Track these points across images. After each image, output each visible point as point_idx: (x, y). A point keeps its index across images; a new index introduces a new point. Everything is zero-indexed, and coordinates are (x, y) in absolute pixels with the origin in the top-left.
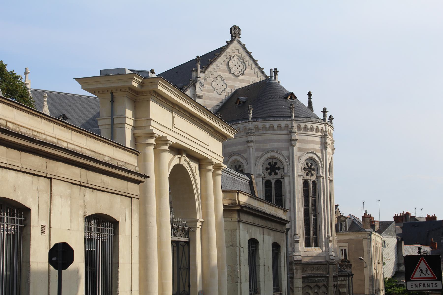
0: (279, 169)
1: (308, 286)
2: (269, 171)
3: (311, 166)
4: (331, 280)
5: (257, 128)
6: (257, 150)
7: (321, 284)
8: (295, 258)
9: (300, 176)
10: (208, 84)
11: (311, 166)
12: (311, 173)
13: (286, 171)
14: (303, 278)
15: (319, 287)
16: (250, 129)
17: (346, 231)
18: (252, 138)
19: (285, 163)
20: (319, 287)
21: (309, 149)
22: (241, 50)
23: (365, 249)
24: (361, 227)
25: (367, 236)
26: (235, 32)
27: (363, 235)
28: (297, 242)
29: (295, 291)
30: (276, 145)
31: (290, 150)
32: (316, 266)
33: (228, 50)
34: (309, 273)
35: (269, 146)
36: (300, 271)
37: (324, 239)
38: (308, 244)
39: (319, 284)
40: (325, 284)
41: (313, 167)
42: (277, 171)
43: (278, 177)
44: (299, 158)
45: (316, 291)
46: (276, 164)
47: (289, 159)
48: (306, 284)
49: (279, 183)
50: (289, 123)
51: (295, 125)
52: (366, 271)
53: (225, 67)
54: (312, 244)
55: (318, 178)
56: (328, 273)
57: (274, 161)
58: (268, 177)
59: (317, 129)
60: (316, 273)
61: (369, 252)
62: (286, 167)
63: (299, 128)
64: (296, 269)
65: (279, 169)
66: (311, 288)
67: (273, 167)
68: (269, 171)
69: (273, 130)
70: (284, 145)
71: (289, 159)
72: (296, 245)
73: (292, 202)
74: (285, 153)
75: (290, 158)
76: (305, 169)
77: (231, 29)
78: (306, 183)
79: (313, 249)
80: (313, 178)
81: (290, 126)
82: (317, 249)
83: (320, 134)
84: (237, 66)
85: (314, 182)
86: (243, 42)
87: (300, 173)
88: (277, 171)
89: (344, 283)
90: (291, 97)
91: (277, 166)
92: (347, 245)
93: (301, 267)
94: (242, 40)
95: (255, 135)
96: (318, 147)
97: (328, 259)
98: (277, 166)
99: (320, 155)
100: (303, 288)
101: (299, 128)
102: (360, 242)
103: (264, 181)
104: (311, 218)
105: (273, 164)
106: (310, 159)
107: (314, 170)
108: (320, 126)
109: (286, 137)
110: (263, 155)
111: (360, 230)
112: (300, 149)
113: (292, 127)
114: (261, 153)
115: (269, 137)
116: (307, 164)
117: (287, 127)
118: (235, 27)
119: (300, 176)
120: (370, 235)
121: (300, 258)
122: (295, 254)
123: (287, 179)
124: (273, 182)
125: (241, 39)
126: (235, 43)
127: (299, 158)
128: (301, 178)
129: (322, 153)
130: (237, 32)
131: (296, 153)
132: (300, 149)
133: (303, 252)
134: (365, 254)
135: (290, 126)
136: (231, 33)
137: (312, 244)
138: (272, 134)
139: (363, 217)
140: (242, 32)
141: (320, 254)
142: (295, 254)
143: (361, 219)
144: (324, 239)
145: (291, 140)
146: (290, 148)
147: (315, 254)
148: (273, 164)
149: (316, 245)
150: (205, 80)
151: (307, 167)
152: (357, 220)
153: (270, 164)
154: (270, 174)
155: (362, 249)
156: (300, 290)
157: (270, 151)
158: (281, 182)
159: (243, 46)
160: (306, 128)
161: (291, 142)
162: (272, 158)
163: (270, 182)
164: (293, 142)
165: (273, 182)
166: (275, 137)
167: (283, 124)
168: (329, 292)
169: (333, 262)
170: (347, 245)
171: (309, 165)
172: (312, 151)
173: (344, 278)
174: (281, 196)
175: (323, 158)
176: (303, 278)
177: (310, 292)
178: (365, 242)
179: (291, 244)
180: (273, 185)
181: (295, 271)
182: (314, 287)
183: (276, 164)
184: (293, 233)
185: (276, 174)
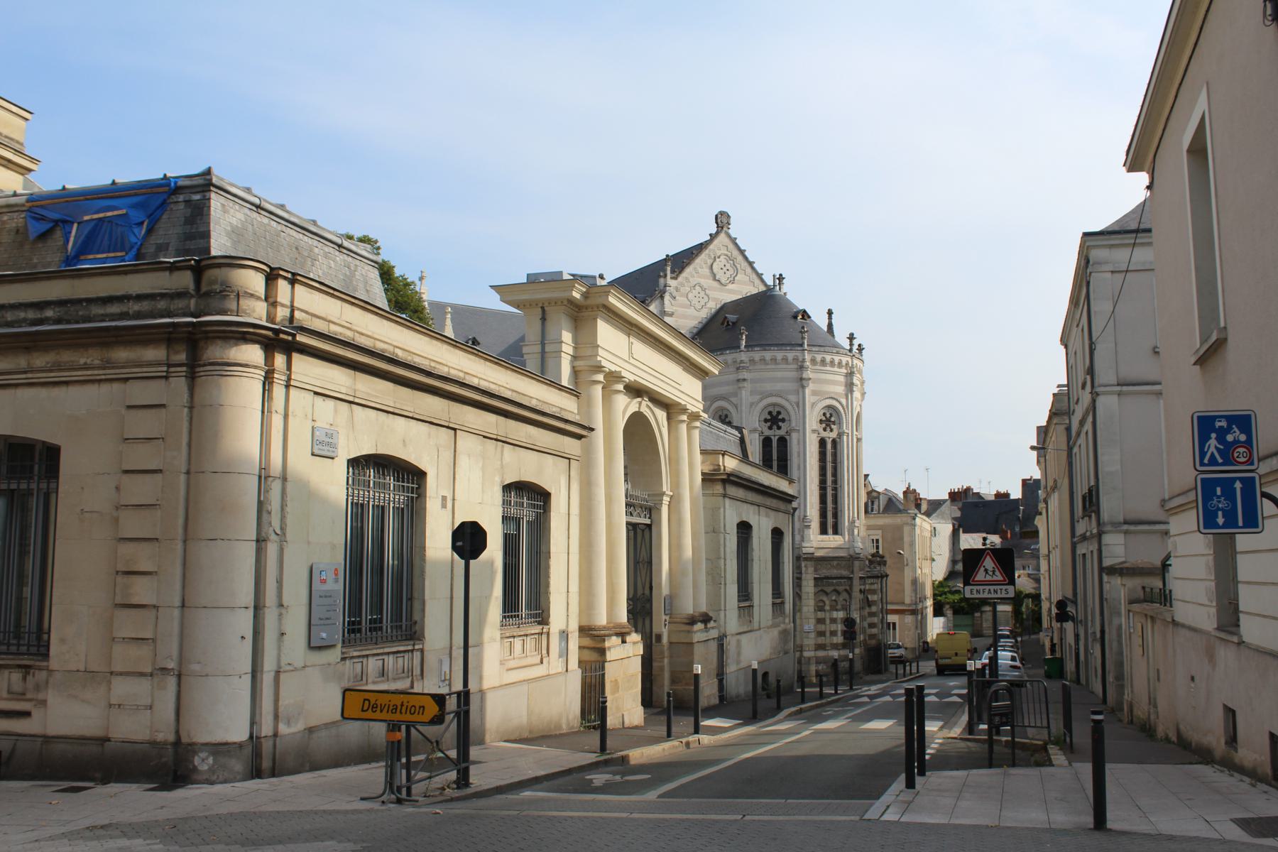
3: (830, 418)
4: (856, 582)
5: (752, 361)
8: (805, 550)
9: (814, 431)
11: (830, 418)
13: (793, 424)
15: (838, 593)
16: (742, 362)
19: (792, 413)
22: (731, 246)
23: (906, 539)
25: (909, 520)
26: (722, 221)
28: (808, 527)
30: (779, 386)
33: (711, 247)
34: (824, 572)
35: (768, 387)
36: (811, 570)
38: (824, 531)
43: (782, 433)
44: (813, 405)
46: (779, 413)
49: (783, 441)
50: (799, 354)
51: (807, 357)
52: (907, 572)
53: (706, 271)
54: (830, 531)
55: (840, 435)
58: (767, 433)
59: (840, 364)
60: (835, 572)
61: (912, 544)
62: (793, 418)
63: (813, 361)
65: (783, 420)
66: (827, 594)
67: (774, 419)
70: (792, 386)
72: (806, 531)
74: (793, 398)
75: (800, 405)
76: (821, 421)
78: (822, 443)
80: (834, 435)
82: (837, 537)
85: (834, 441)
86: (733, 236)
87: (815, 427)
89: (875, 587)
94: (733, 232)
95: (750, 371)
96: (841, 389)
99: (844, 401)
101: (813, 361)
102: (899, 529)
104: (830, 492)
106: (829, 407)
108: (845, 359)
109: (794, 374)
110: (761, 400)
111: (900, 511)
112: (814, 393)
113: (804, 360)
117: (796, 359)
118: (722, 213)
119: (814, 431)
121: (811, 550)
123: (794, 435)
124: (775, 440)
126: (722, 235)
127: (813, 405)
132: (814, 393)
133: (816, 542)
134: (906, 546)
137: (830, 531)
138: (773, 370)
140: (732, 221)
141: (383, 350)
143: (901, 496)
145: (801, 379)
149: (836, 532)
150: (677, 289)
152: (895, 496)
153: (770, 413)
154: (770, 428)
155: (902, 538)
156: (811, 596)
157: (771, 395)
159: (734, 241)
160: (823, 362)
161: (802, 382)
162: (774, 405)
164: (805, 383)
165: (775, 440)
166: (779, 374)
167: (790, 355)
177: (825, 599)
178: (906, 529)
180: (775, 444)
183: (779, 413)
185: (779, 428)
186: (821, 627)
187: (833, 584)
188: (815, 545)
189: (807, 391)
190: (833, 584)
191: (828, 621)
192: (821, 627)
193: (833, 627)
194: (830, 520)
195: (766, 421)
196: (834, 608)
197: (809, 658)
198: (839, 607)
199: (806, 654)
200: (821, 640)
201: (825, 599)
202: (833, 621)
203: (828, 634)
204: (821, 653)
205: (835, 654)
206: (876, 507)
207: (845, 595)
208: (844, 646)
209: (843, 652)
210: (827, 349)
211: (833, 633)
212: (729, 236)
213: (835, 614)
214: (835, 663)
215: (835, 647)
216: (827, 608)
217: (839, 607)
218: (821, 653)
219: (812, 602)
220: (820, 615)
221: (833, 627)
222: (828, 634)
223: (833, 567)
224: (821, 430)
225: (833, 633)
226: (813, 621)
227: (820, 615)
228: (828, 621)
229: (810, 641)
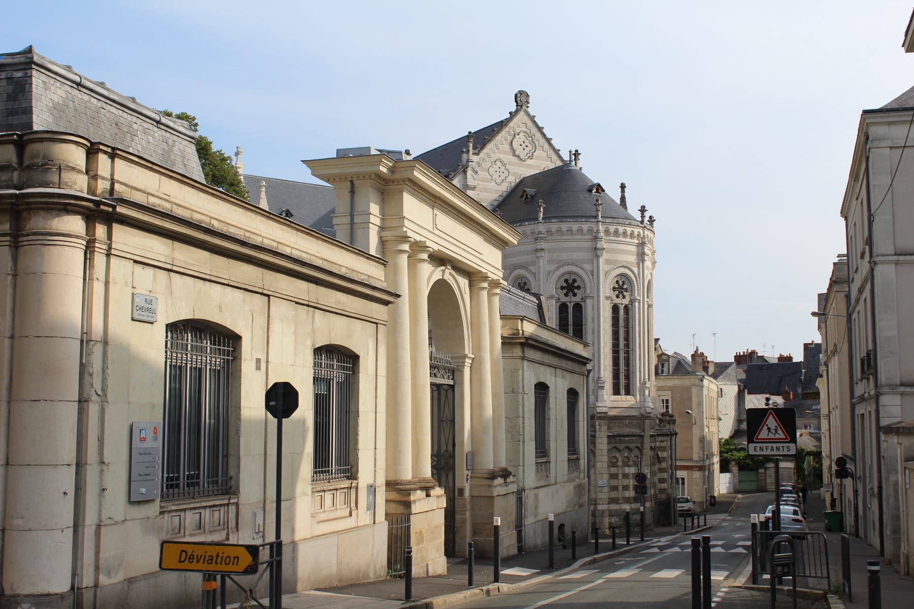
0: (579, 288)
1: (615, 447)
2: (565, 291)
3: (622, 286)
4: (647, 440)
5: (549, 232)
6: (549, 262)
7: (632, 446)
8: (599, 410)
9: (607, 298)
10: (483, 170)
13: (588, 291)
14: (608, 436)
15: (630, 450)
16: (540, 233)
17: (668, 375)
18: (542, 245)
20: (630, 450)
21: (620, 262)
22: (530, 124)
23: (695, 399)
24: (690, 370)
25: (697, 382)
26: (521, 100)
27: (693, 380)
28: (602, 388)
30: (575, 256)
31: (595, 262)
32: (627, 422)
33: (511, 124)
34: (617, 431)
35: (565, 256)
36: (604, 428)
37: (638, 385)
38: (616, 392)
39: (629, 445)
40: (639, 445)
41: (625, 287)
42: (576, 291)
43: (577, 299)
44: (607, 273)
45: (626, 455)
46: (574, 281)
47: (592, 275)
48: (613, 445)
49: (578, 307)
50: (593, 226)
51: (602, 228)
52: (695, 429)
53: (507, 147)
54: (622, 391)
55: (632, 301)
56: (644, 431)
57: (573, 277)
58: (564, 299)
60: (627, 431)
61: (700, 404)
62: (588, 285)
63: (607, 232)
64: (599, 425)
65: (579, 288)
66: (619, 450)
67: (570, 286)
68: (565, 291)
69: (572, 235)
70: (587, 255)
71: (592, 275)
72: (600, 392)
73: (596, 333)
74: (587, 267)
77: (516, 95)
78: (615, 308)
79: (624, 397)
80: (626, 301)
81: (595, 230)
82: (628, 397)
83: (636, 241)
84: (524, 146)
85: (626, 307)
86: (532, 114)
87: (608, 294)
88: (576, 291)
90: (597, 190)
91: (576, 285)
92: (669, 393)
93: (606, 421)
96: (633, 259)
97: (643, 412)
98: (576, 285)
99: (635, 270)
100: (609, 451)
101: (607, 232)
102: (688, 389)
103: (558, 304)
104: (622, 355)
105: (570, 281)
106: (622, 275)
107: (626, 290)
109: (588, 244)
110: (559, 268)
111: (688, 373)
112: (608, 262)
113: (598, 231)
114: (555, 266)
115: (565, 245)
116: (617, 282)
117: (590, 230)
118: (521, 93)
119: (607, 298)
120: (702, 381)
121: (605, 410)
122: (598, 404)
124: (571, 306)
125: (529, 110)
127: (607, 273)
128: (609, 301)
129: (639, 267)
130: (524, 100)
131: (603, 267)
132: (608, 262)
133: (610, 401)
134: (694, 406)
135: (595, 230)
136: (516, 101)
137: (622, 391)
139: (693, 356)
140: (530, 100)
142: (598, 404)
143: (690, 359)
144: (638, 385)
145: (596, 249)
146: (595, 259)
147: (625, 405)
148: (570, 281)
149: (628, 393)
151: (617, 286)
154: (566, 295)
155: (690, 399)
156: (605, 453)
158: (581, 307)
160: (616, 232)
161: (596, 252)
162: (570, 273)
163: (567, 306)
164: (599, 252)
165: (571, 306)
166: (574, 244)
167: (585, 227)
170: (669, 393)
171: (621, 283)
172: (625, 264)
173: (665, 438)
174: (582, 325)
175: (639, 274)
176: (608, 436)
177: (618, 455)
178: (694, 390)
179: (594, 391)
180: (570, 310)
181: (597, 427)
183: (574, 281)
184: (596, 376)
185: (575, 295)
186: (614, 482)
187: (625, 442)
188: (608, 404)
189: (601, 260)
190: (625, 442)
191: (620, 476)
192: (614, 482)
193: (626, 482)
194: (622, 381)
195: (562, 288)
196: (626, 464)
197: (603, 512)
198: (631, 463)
199: (600, 507)
200: (614, 494)
201: (618, 455)
202: (626, 476)
203: (620, 488)
204: (614, 507)
205: (627, 507)
206: (665, 369)
207: (636, 452)
208: (636, 500)
209: (634, 506)
210: (620, 221)
211: (626, 488)
212: (528, 114)
214: (627, 516)
215: (627, 500)
216: (620, 464)
217: (631, 463)
218: (614, 507)
219: (605, 459)
220: (613, 470)
221: (626, 482)
222: (620, 488)
223: (625, 425)
224: (614, 297)
225: (626, 488)
226: (606, 477)
227: (613, 470)
228: (620, 476)
229: (604, 495)
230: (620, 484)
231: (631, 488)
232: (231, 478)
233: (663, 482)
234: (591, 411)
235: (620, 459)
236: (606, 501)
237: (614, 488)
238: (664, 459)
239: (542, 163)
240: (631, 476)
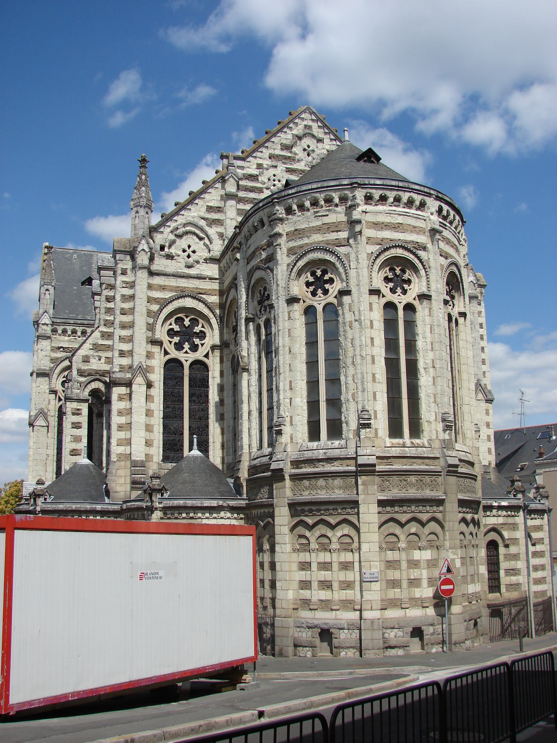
1: (392, 520)
12: (403, 288)
29: (361, 531)
32: (413, 479)
34: (395, 493)
38: (395, 430)
45: (413, 530)
48: (388, 516)
60: (412, 493)
63: (368, 198)
66: (402, 525)
85: (409, 308)
88: (327, 286)
91: (320, 291)
93: (377, 479)
98: (320, 291)
113: (354, 198)
124: (320, 308)
133: (378, 443)
154: (314, 294)
168: (447, 533)
169: (456, 472)
182: (408, 522)
185: (326, 292)
191: (404, 565)
193: (414, 574)
196: (412, 546)
197: (372, 621)
202: (414, 564)
203: (405, 584)
204: (393, 614)
207: (433, 526)
211: (414, 583)
213: (417, 555)
218: (393, 614)
220: (391, 555)
222: (405, 584)
223: (412, 485)
227: (391, 555)
228: (404, 565)
230: (405, 576)
231: (425, 583)
232: (204, 182)
233: (515, 575)
234: (247, 666)
235: (402, 537)
236: (377, 605)
237: (394, 584)
238: (515, 541)
239: (148, 318)
240: (423, 564)
